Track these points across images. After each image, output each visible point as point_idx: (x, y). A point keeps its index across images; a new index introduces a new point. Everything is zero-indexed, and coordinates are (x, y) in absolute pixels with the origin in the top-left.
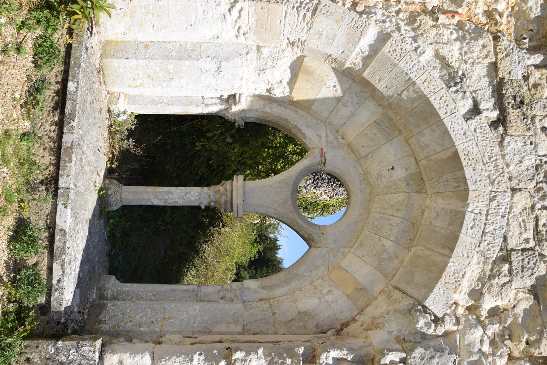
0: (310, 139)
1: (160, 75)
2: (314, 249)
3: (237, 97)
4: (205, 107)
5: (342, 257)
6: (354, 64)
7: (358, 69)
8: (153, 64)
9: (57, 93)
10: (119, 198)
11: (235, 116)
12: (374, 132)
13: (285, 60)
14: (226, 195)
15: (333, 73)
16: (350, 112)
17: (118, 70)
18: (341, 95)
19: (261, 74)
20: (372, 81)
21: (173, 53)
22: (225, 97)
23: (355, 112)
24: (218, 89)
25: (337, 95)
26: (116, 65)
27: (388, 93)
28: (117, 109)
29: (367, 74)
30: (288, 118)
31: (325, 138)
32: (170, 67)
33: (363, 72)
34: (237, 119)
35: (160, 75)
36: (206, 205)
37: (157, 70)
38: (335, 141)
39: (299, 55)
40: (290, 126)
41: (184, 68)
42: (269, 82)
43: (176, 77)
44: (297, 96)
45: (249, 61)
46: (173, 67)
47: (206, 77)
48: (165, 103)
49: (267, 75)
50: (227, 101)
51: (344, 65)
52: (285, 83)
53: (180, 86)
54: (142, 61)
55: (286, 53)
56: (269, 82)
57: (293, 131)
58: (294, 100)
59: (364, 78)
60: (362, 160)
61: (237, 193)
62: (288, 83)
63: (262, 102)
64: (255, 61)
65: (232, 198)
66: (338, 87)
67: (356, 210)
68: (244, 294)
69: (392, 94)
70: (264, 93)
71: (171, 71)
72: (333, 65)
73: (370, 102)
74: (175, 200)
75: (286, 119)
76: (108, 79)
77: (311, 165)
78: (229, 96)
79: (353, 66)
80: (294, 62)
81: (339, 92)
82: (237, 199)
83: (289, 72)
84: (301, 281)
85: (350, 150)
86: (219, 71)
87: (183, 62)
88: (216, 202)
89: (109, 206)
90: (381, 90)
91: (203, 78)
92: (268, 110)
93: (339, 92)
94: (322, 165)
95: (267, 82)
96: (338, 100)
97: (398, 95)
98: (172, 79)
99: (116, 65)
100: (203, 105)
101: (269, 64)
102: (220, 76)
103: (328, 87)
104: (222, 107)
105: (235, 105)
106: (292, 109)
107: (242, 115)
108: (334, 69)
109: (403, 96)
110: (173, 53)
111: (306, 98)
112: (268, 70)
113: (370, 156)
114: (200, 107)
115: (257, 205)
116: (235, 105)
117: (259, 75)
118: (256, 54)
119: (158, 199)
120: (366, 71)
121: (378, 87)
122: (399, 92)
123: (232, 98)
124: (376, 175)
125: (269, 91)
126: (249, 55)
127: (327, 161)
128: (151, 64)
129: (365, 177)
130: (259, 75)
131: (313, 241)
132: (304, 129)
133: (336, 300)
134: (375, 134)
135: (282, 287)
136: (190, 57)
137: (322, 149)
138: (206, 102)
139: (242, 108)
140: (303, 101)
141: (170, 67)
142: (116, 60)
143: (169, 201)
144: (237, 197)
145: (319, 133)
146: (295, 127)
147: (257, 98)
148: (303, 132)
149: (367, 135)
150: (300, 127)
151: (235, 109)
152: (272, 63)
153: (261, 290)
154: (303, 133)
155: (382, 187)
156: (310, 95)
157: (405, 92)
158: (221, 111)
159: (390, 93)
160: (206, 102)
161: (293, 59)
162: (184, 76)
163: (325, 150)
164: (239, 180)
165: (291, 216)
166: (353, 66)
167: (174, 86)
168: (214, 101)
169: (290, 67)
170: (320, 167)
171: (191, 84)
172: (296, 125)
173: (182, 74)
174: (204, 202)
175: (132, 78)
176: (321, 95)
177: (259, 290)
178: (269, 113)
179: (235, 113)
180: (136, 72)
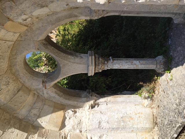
0: (52, 92)
1: (127, 119)
2: (43, 39)
3: (91, 108)
4: (106, 101)
5: (21, 35)
6: (33, 137)
7: (31, 136)
8: (130, 126)
9: (183, 132)
10: (158, 65)
11: (92, 98)
12: (16, 106)
13: (68, 129)
14: (98, 69)
15: (44, 127)
16: (32, 112)
17: (147, 122)
18: (38, 120)
19: (80, 121)
20: (21, 132)
21: (120, 130)
22: (96, 106)
23: (29, 113)
24: (100, 113)
25: (40, 119)
26: (147, 124)
27: (11, 129)
28: (149, 101)
29: (25, 135)
30: (65, 100)
31: (44, 93)
32: (122, 124)
33: (27, 135)
34: (91, 97)
35: (127, 119)
36: (109, 61)
37: (128, 122)
38: (39, 92)
39: (61, 131)
40: (64, 96)
41: (116, 123)
42: (76, 117)
43: (120, 119)
44: (61, 113)
45: (85, 127)
46: (121, 124)
47: (106, 120)
48: (125, 102)
49: (76, 121)
50: (95, 105)
51: (39, 136)
52: (68, 118)
53: (118, 114)
54: (135, 127)
55: (68, 131)
56: (76, 117)
57: (62, 93)
58: (63, 111)
59: (26, 133)
60: (20, 86)
61: (92, 71)
62: (66, 118)
63: (79, 105)
64: (82, 127)
65: (95, 67)
66: (40, 123)
67: (19, 60)
68: (89, 12)
69: (9, 130)
70: (77, 110)
71: (122, 122)
72: (44, 130)
73: (21, 118)
74: (127, 64)
75: (66, 99)
76: (152, 117)
77: (51, 82)
78: (94, 107)
79: (33, 136)
80: (64, 128)
81: (39, 120)
82: (92, 68)
83: (66, 124)
84: (49, 20)
85: (29, 88)
86: (100, 123)
87: (116, 127)
88: (104, 64)
89: (165, 62)
90: (16, 130)
91: (107, 119)
92: (76, 102)
93: (39, 120)
94: (44, 81)
95: (77, 117)
96: (39, 117)
97: (5, 131)
98: (122, 118)
99: (147, 124)
100: (107, 102)
101: (76, 127)
102: (99, 120)
103: (45, 122)
104: (98, 101)
105: (92, 104)
106: (63, 103)
107: (88, 99)
108: (43, 128)
109: (2, 132)
110: (120, 130)
111: (57, 113)
112: (76, 124)
113: (16, 92)
114: (109, 101)
115: (80, 64)
116: (92, 104)
117: (80, 120)
118: (82, 130)
119: (136, 64)
120: (26, 136)
121: (18, 131)
122: (5, 133)
123: (93, 107)
124: (10, 84)
125: (75, 112)
126: (85, 130)
127: (42, 83)
128: (131, 125)
129: (17, 78)
130: (80, 120)
131: (44, 44)
132: (57, 96)
133: (18, 16)
134: (15, 105)
135: (62, 16)
136: (113, 129)
137: (46, 88)
138: (106, 103)
139: (88, 102)
140: (58, 111)
141: (122, 124)
142: (147, 127)
143: (130, 64)
144: (92, 69)
145: (48, 95)
146: (61, 96)
147: (81, 106)
148: (57, 95)
149: (20, 103)
150: (58, 97)
151: (92, 102)
152: (75, 127)
153: (78, 15)
154: (57, 94)
155: (4, 78)
156: (54, 115)
157: (1, 134)
158: (98, 99)
159: (10, 130)
160: (106, 103)
161: (64, 129)
162: (116, 120)
163: (44, 88)
164: (91, 73)
165: (60, 59)
166: (33, 136)
167: (121, 114)
168: (102, 103)
169: (66, 126)
170: (46, 80)
171: (113, 115)
172: (61, 97)
173: (117, 120)
174: (110, 63)
175: (141, 117)
176: (49, 117)
177: (79, 15)
178: (75, 101)
179: (92, 100)
180: (138, 121)
